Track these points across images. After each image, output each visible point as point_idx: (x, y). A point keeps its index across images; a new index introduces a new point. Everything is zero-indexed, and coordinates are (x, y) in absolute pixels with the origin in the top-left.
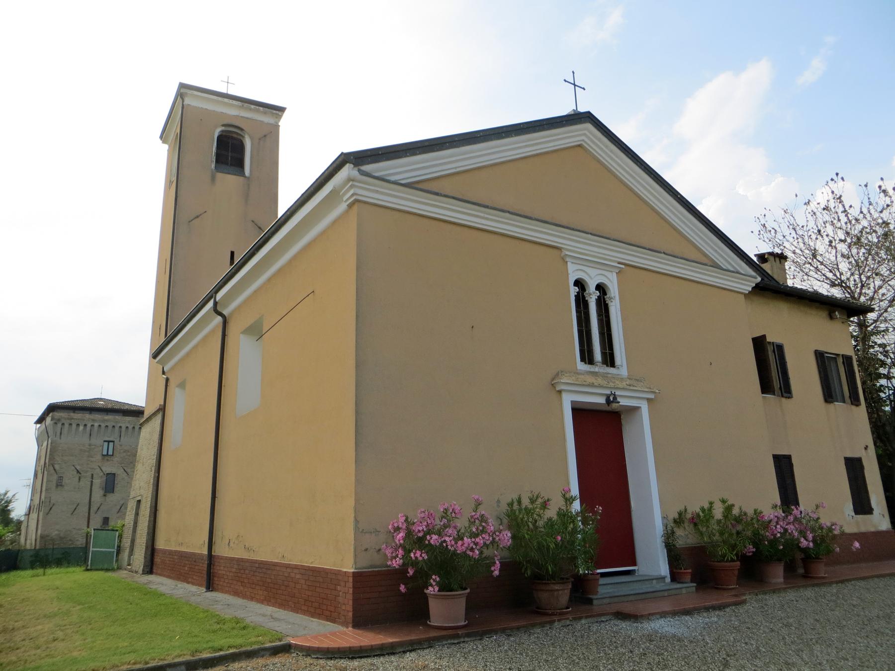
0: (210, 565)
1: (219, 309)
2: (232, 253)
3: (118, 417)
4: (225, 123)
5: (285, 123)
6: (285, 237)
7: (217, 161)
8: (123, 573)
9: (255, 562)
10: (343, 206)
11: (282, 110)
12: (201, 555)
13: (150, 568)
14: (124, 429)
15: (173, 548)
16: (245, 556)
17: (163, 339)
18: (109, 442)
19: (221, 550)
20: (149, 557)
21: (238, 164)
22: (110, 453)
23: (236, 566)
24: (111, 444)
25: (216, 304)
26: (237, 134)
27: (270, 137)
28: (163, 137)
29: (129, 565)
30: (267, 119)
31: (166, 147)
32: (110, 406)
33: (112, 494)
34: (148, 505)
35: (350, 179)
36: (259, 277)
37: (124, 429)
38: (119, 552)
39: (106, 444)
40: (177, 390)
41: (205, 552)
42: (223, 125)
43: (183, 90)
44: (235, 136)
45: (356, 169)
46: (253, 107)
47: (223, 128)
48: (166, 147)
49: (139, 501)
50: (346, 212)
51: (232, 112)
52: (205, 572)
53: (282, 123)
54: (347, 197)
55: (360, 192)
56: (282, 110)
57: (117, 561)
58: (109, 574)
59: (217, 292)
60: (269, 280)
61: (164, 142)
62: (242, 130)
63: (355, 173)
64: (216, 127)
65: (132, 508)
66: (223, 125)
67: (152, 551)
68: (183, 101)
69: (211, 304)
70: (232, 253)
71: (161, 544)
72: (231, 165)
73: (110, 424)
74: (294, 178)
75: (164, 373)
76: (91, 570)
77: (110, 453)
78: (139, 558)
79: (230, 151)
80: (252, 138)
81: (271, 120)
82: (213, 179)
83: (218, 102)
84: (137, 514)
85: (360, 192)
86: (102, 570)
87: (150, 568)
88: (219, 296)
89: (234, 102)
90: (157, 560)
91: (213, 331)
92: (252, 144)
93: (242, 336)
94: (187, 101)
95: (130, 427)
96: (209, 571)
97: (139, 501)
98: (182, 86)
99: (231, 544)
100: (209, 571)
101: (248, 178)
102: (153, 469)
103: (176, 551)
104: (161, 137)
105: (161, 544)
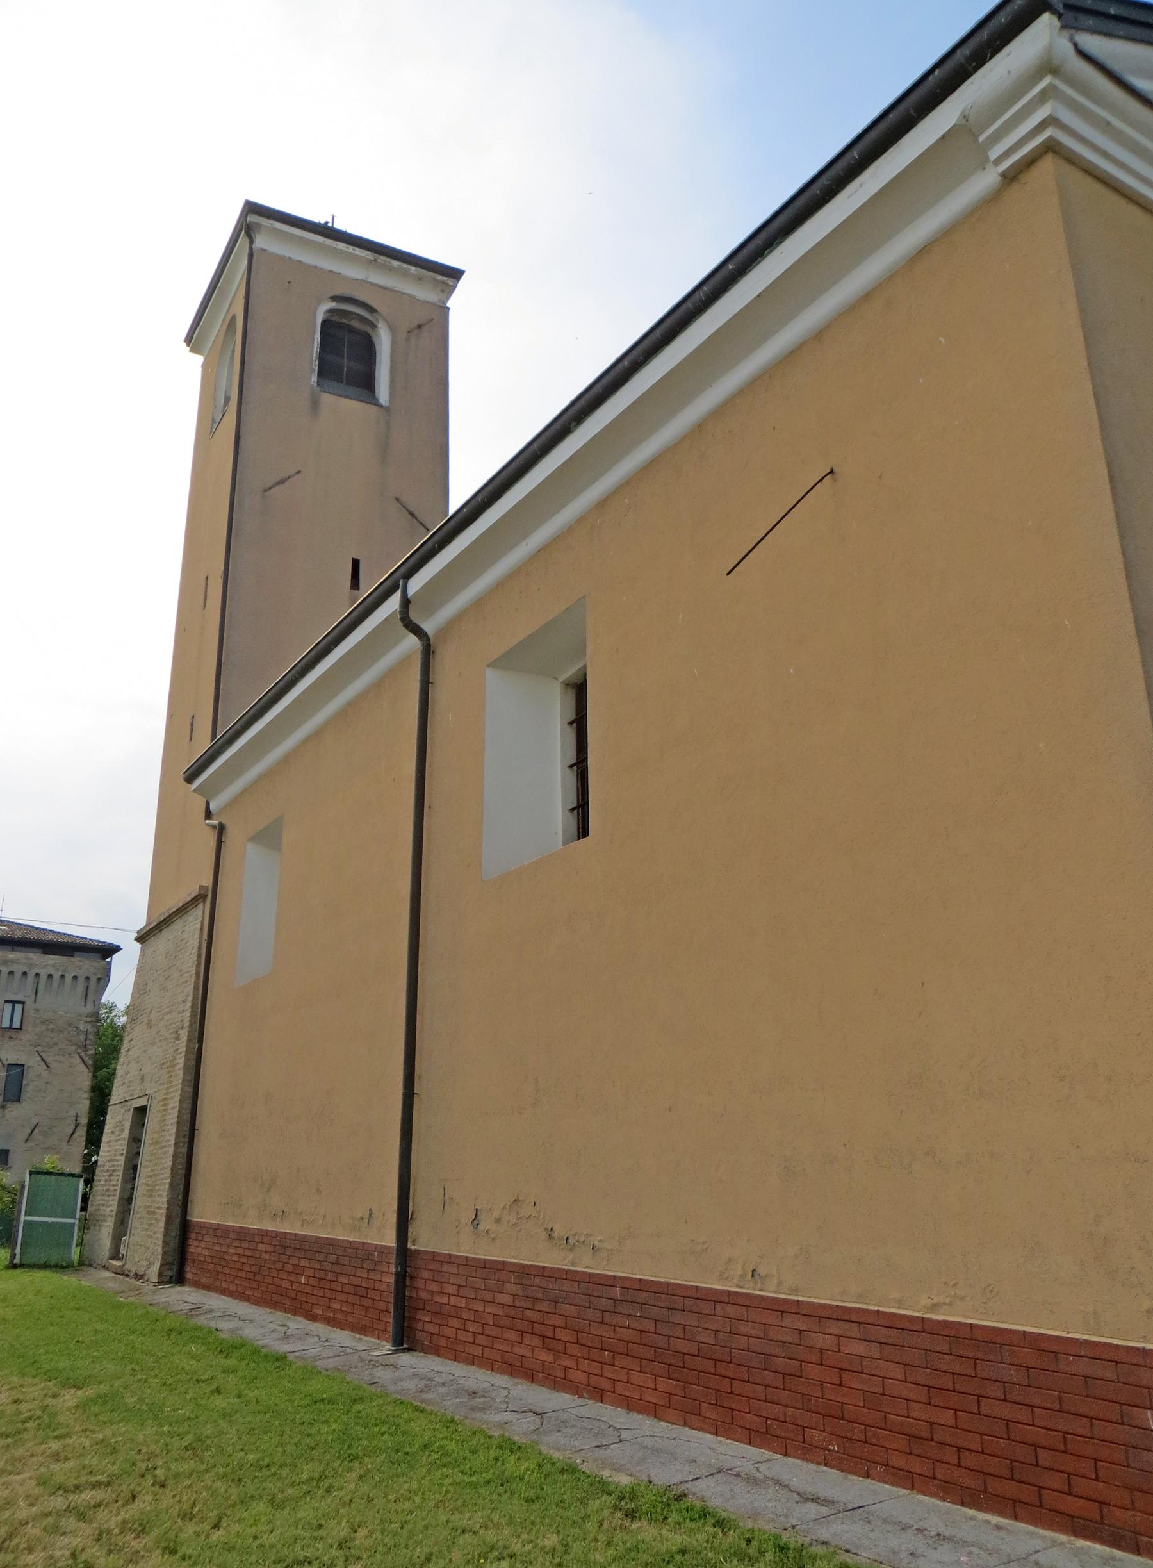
0: (403, 1278)
1: (414, 616)
2: (356, 564)
3: (35, 957)
4: (338, 293)
5: (461, 304)
6: (993, 123)
7: (321, 374)
8: (102, 1279)
9: (612, 1282)
10: (986, 180)
11: (456, 274)
12: (363, 1253)
13: (177, 1270)
14: (43, 977)
15: (253, 1223)
16: (554, 1259)
17: (204, 744)
18: (14, 1003)
19: (423, 1239)
20: (174, 1244)
21: (365, 384)
22: (16, 1024)
23: (512, 1288)
24: (18, 1007)
25: (406, 602)
26: (363, 319)
27: (430, 333)
28: (193, 339)
29: (115, 1256)
30: (424, 293)
31: (199, 359)
32: (18, 934)
33: (17, 1105)
34: (172, 1117)
35: (1048, 67)
36: (562, 507)
37: (43, 977)
38: (85, 1225)
39: (9, 1007)
40: (252, 849)
41: (389, 1239)
42: (334, 298)
43: (252, 218)
44: (356, 324)
45: (1066, 33)
46: (395, 263)
47: (333, 305)
48: (199, 359)
49: (141, 1111)
50: (993, 198)
51: (353, 271)
52: (391, 1298)
53: (454, 303)
54: (1013, 141)
55: (1067, 116)
56: (456, 274)
57: (79, 1245)
58: (69, 1280)
59: (408, 575)
60: (601, 505)
61: (195, 350)
62: (372, 310)
63: (1064, 46)
64: (319, 301)
65: (120, 1125)
66: (334, 298)
67: (182, 1230)
68: (251, 242)
69: (393, 603)
70: (356, 564)
71: (206, 1210)
72: (348, 383)
73: (18, 969)
74: (495, 401)
75: (208, 815)
76: (21, 1266)
77: (16, 1024)
78: (147, 1243)
79: (345, 353)
80: (392, 328)
81: (432, 296)
82: (315, 405)
83: (321, 246)
84: (136, 1140)
85: (1067, 116)
86: (45, 1266)
87: (177, 1270)
88: (415, 584)
89: (358, 251)
90: (196, 1248)
91: (393, 672)
92: (394, 343)
93: (490, 673)
94: (260, 242)
95: (56, 976)
96: (407, 1299)
97: (141, 1111)
98: (251, 208)
99: (485, 1224)
100: (407, 1299)
101: (387, 409)
102: (184, 1035)
103: (263, 1234)
104: (189, 340)
105: (204, 1212)
